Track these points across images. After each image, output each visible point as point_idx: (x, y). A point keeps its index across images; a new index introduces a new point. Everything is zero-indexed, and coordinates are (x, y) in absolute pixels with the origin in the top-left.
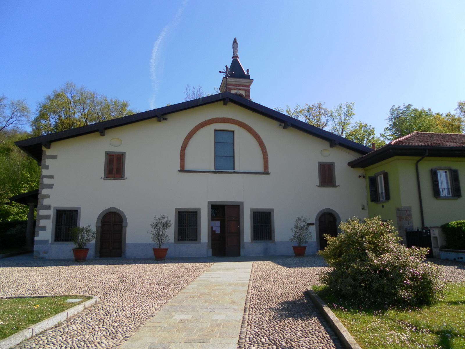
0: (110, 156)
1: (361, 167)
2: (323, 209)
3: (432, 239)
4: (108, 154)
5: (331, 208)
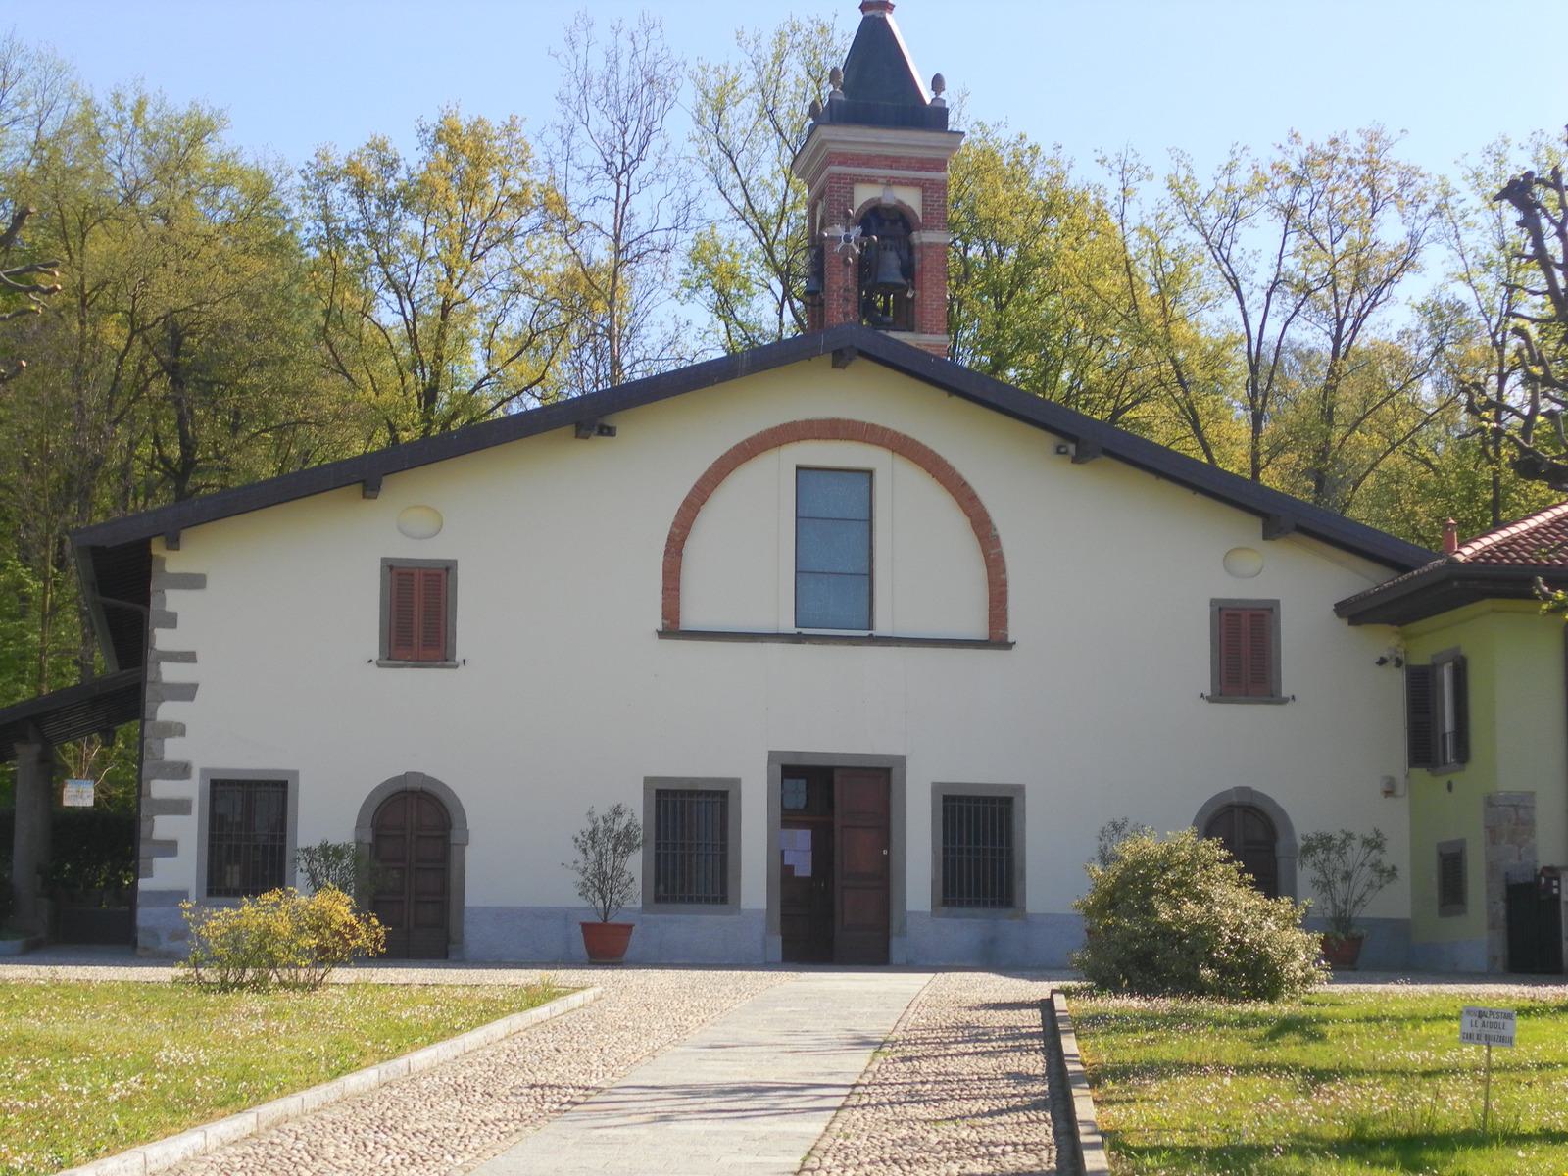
0: (400, 574)
1: (1392, 623)
2: (1227, 788)
3: (1563, 905)
4: (391, 568)
5: (1256, 787)
